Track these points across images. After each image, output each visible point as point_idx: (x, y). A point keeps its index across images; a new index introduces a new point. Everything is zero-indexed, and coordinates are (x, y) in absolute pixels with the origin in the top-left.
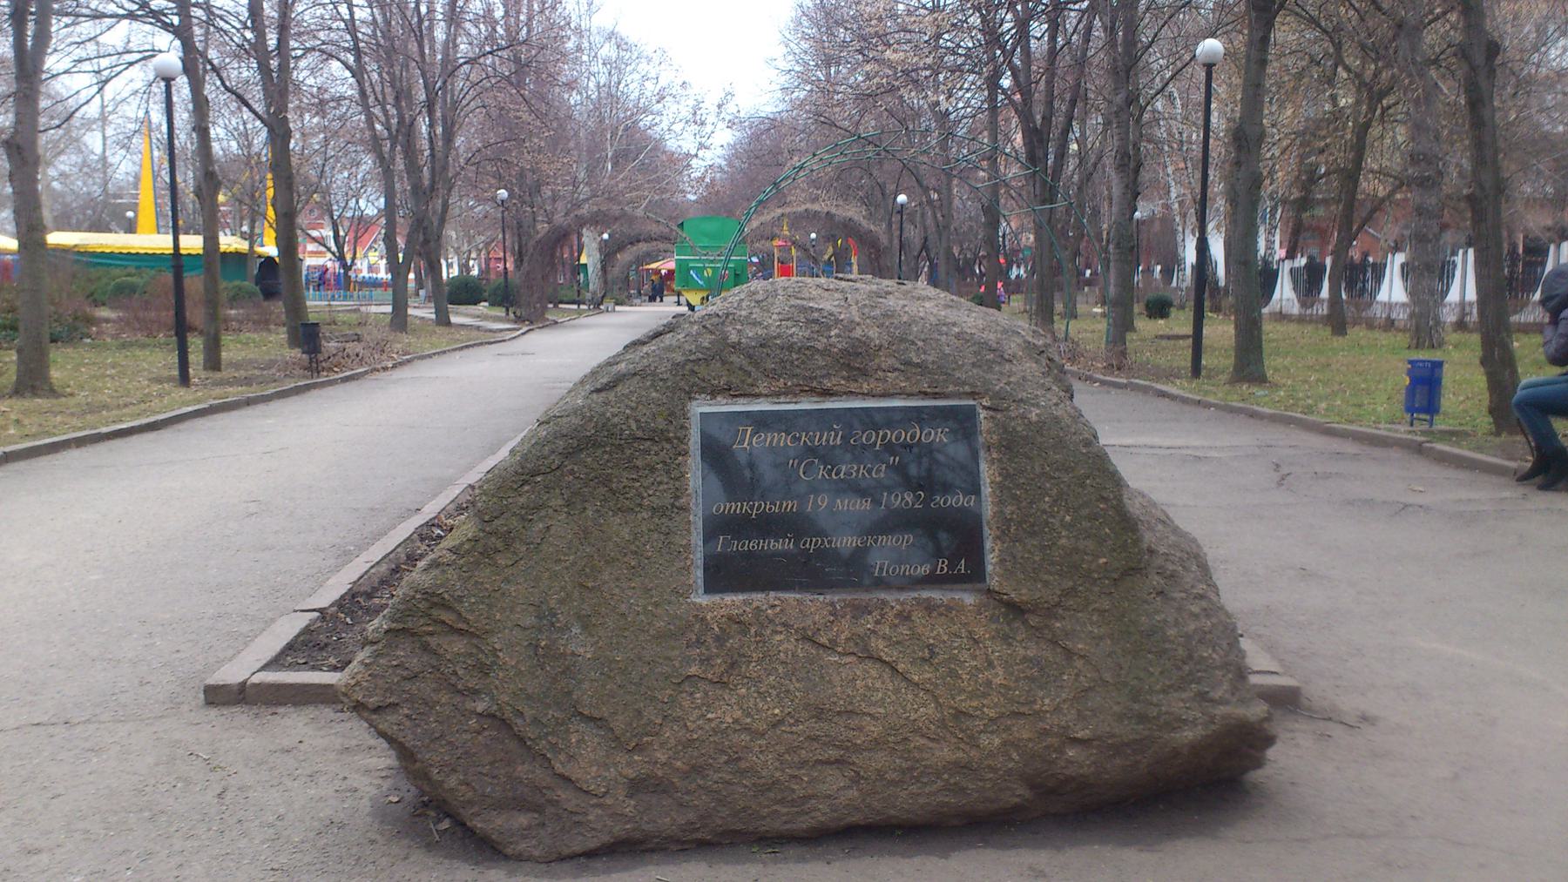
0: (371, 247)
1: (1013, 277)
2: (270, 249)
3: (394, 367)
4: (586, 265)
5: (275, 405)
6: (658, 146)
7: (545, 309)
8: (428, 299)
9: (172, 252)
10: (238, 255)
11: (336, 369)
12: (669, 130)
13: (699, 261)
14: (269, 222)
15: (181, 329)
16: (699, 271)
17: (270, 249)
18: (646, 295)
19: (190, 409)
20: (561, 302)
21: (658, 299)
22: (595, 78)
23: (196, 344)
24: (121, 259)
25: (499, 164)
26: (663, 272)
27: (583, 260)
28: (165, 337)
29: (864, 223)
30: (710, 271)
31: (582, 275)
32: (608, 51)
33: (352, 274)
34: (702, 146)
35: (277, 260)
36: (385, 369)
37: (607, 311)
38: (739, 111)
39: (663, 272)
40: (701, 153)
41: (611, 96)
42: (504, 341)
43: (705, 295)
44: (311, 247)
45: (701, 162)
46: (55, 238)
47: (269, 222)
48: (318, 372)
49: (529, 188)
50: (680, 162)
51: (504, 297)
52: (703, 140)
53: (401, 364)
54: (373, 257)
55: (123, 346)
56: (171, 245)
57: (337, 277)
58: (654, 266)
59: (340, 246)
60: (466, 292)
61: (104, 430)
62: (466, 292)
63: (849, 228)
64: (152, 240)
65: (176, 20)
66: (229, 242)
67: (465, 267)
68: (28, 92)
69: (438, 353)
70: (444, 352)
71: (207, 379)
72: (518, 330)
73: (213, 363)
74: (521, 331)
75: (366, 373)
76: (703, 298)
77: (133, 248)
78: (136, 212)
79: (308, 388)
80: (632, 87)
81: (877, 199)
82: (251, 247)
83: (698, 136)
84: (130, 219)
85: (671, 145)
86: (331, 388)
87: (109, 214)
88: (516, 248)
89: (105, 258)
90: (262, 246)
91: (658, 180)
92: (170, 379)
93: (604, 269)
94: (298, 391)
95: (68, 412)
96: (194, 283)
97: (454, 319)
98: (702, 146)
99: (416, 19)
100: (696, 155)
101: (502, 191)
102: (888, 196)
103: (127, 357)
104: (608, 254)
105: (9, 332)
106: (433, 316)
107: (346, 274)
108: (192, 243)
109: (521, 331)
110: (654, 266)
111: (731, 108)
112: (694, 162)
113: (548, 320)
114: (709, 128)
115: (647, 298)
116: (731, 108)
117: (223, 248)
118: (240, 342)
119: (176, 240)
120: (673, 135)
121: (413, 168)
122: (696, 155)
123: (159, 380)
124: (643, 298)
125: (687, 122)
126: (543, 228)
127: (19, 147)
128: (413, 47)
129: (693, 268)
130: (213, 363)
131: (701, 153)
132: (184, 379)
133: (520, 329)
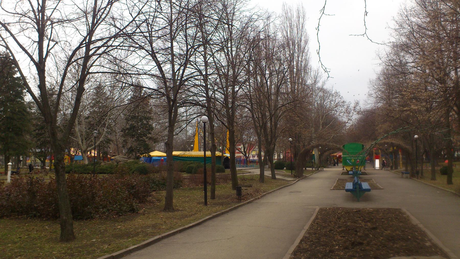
0: (253, 150)
1: (456, 155)
2: (228, 155)
3: (261, 197)
4: (314, 154)
5: (230, 214)
6: (336, 119)
7: (302, 170)
8: (269, 167)
9: (203, 156)
10: (219, 157)
11: (245, 199)
12: (339, 115)
13: (349, 157)
14: (227, 148)
15: (205, 183)
16: (350, 160)
17: (228, 155)
18: (332, 164)
19: (208, 217)
20: (307, 167)
21: (336, 165)
22: (317, 101)
23: (209, 188)
24: (190, 158)
25: (289, 132)
26: (338, 156)
27: (313, 153)
28: (201, 186)
29: (404, 145)
30: (353, 160)
31: (313, 160)
32: (321, 94)
33: (248, 159)
34: (349, 119)
35: (229, 158)
36: (259, 198)
37: (321, 171)
38: (360, 109)
39: (338, 156)
40: (349, 122)
41: (321, 106)
42: (291, 185)
43: (352, 167)
44: (237, 151)
45: (349, 124)
46: (175, 153)
47: (227, 148)
48: (241, 200)
49: (297, 138)
50: (343, 124)
51: (291, 168)
52: (350, 118)
53: (263, 196)
54: (254, 153)
55: (191, 189)
56: (203, 154)
57: (244, 160)
58: (335, 154)
59: (245, 152)
60: (279, 166)
61: (186, 226)
62: (279, 166)
63: (399, 147)
64: (197, 153)
65: (204, 85)
66: (218, 153)
67: (279, 156)
68: (171, 130)
69: (273, 191)
70: (275, 191)
71: (211, 202)
72: (295, 180)
73: (213, 197)
74: (296, 181)
75: (253, 200)
76: (351, 168)
77: (192, 155)
78: (194, 145)
79: (238, 207)
80: (327, 103)
81: (407, 137)
82: (222, 154)
83: (348, 117)
84: (192, 147)
85: (340, 119)
86: (244, 206)
87: (188, 145)
88: (294, 153)
89: (186, 158)
90: (225, 154)
91: (336, 130)
92: (202, 203)
93: (320, 158)
94: (236, 208)
95: (177, 218)
96: (209, 166)
97: (277, 177)
98: (349, 119)
99: (267, 96)
100: (348, 122)
101: (290, 139)
102: (410, 135)
103: (191, 193)
104: (322, 153)
105: (163, 186)
106: (271, 176)
107: (247, 159)
108: (208, 153)
109: (296, 181)
110: (335, 154)
111: (358, 108)
112: (347, 124)
113: (304, 176)
114: (351, 114)
115: (333, 165)
116: (358, 108)
117: (216, 155)
118: (220, 188)
119: (205, 153)
120: (340, 116)
121: (266, 135)
122: (348, 122)
123: (199, 203)
124: (332, 165)
125: (344, 113)
126: (302, 150)
127: (168, 144)
128: (267, 102)
129: (348, 159)
130: (213, 197)
131: (349, 122)
132: (206, 203)
133: (296, 180)
